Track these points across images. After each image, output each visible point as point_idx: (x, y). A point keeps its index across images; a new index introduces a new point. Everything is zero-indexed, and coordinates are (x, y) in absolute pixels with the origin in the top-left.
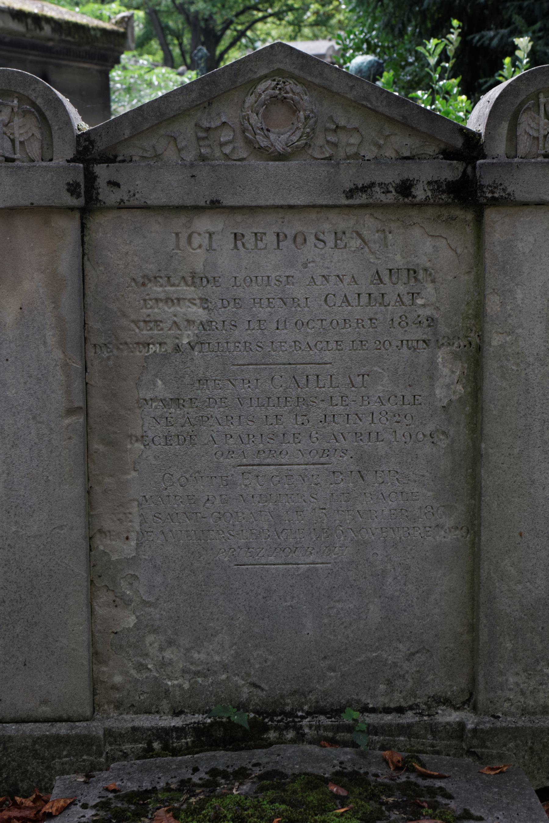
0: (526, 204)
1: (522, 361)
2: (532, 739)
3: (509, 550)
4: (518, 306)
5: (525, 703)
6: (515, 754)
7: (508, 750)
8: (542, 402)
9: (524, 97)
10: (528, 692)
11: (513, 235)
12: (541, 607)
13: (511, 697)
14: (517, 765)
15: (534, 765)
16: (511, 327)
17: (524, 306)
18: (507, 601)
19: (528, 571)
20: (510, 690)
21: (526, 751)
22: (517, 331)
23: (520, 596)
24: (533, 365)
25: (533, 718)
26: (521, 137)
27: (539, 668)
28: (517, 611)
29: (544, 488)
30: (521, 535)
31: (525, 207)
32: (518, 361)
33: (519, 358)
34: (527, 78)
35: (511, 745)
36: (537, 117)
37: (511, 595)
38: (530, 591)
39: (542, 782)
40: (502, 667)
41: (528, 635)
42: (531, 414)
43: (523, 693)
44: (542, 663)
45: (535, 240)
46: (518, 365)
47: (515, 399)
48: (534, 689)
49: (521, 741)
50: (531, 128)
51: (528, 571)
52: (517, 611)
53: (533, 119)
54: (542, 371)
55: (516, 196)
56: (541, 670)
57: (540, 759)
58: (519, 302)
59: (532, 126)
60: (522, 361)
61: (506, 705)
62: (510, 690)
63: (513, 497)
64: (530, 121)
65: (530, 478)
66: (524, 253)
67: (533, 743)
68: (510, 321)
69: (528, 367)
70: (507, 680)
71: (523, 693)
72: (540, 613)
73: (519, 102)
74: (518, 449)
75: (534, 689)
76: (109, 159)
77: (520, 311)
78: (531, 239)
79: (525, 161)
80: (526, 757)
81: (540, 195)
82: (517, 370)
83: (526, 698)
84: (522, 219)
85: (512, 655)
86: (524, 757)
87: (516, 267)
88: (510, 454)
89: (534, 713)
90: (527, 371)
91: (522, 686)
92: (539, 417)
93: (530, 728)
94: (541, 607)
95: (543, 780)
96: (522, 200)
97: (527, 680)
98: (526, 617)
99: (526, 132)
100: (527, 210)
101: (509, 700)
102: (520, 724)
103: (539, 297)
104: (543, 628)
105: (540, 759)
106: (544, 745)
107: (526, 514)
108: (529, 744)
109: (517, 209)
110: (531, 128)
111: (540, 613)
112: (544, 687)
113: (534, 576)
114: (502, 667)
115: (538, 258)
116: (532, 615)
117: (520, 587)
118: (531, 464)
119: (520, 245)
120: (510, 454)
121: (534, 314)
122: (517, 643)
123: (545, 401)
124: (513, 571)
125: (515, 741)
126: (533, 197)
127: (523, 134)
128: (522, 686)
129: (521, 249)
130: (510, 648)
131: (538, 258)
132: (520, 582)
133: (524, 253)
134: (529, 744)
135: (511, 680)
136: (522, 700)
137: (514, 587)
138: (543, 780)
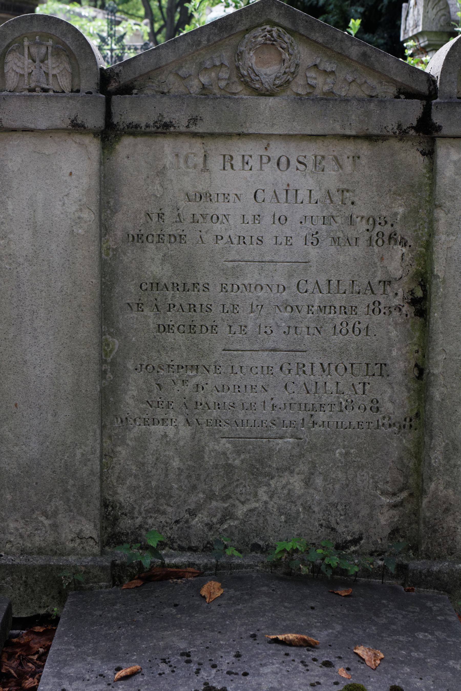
0: (14, 130)
1: (13, 262)
2: (26, 574)
3: (7, 418)
4: (9, 215)
5: (23, 545)
6: (12, 586)
7: (6, 583)
8: (31, 296)
9: (10, 40)
10: (26, 536)
11: (4, 155)
12: (35, 466)
13: (12, 540)
14: (14, 596)
15: (28, 596)
16: (3, 233)
17: (14, 215)
18: (6, 460)
19: (23, 436)
20: (11, 533)
21: (21, 584)
22: (9, 236)
23: (17, 456)
24: (23, 264)
25: (29, 557)
26: (9, 74)
27: (34, 516)
28: (15, 468)
29: (34, 368)
30: (16, 405)
31: (13, 133)
32: (11, 261)
33: (11, 259)
34: (12, 24)
35: (9, 579)
36: (22, 57)
37: (10, 455)
38: (25, 452)
39: (35, 610)
40: (4, 514)
41: (25, 489)
42: (22, 306)
43: (21, 536)
44: (37, 512)
45: (22, 161)
46: (10, 264)
47: (9, 292)
48: (31, 533)
49: (17, 576)
50: (18, 67)
51: (23, 436)
52: (15, 468)
53: (19, 59)
54: (31, 270)
55: (3, 123)
56: (37, 518)
57: (33, 591)
58: (10, 212)
59: (18, 65)
60: (13, 262)
61: (8, 546)
62: (11, 533)
63: (9, 374)
64: (17, 61)
65: (23, 359)
66: (13, 171)
67: (27, 578)
68: (3, 228)
69: (19, 266)
70: (8, 525)
71: (21, 536)
72: (34, 471)
73: (6, 44)
74: (12, 334)
75: (31, 533)
76: (126, 90)
77: (11, 219)
78: (19, 160)
79: (11, 94)
80: (21, 589)
81: (23, 123)
82: (10, 269)
83: (24, 541)
84: (11, 143)
85: (11, 505)
86: (19, 589)
87: (7, 183)
88: (5, 339)
89: (31, 553)
90: (18, 269)
91: (21, 531)
92: (29, 308)
93: (24, 565)
94: (35, 466)
95: (36, 608)
96: (9, 126)
97: (25, 526)
98: (22, 474)
99: (13, 70)
100: (15, 135)
101: (11, 542)
102: (18, 561)
103: (27, 208)
104: (36, 483)
105: (33, 591)
106: (36, 580)
107: (20, 388)
108: (24, 578)
109: (6, 134)
110: (18, 67)
111: (34, 471)
112: (39, 532)
113: (28, 440)
114: (4, 514)
115: (24, 175)
116: (27, 472)
117: (17, 449)
118: (23, 348)
119: (10, 164)
120: (5, 339)
121: (23, 222)
122: (16, 495)
123: (33, 295)
124: (10, 436)
125: (12, 575)
126: (17, 124)
127: (11, 71)
128: (21, 531)
129: (11, 168)
130: (10, 499)
131: (24, 175)
132: (17, 445)
133: (13, 171)
134: (24, 578)
135: (12, 525)
136: (21, 542)
137: (12, 449)
138: (36, 608)
